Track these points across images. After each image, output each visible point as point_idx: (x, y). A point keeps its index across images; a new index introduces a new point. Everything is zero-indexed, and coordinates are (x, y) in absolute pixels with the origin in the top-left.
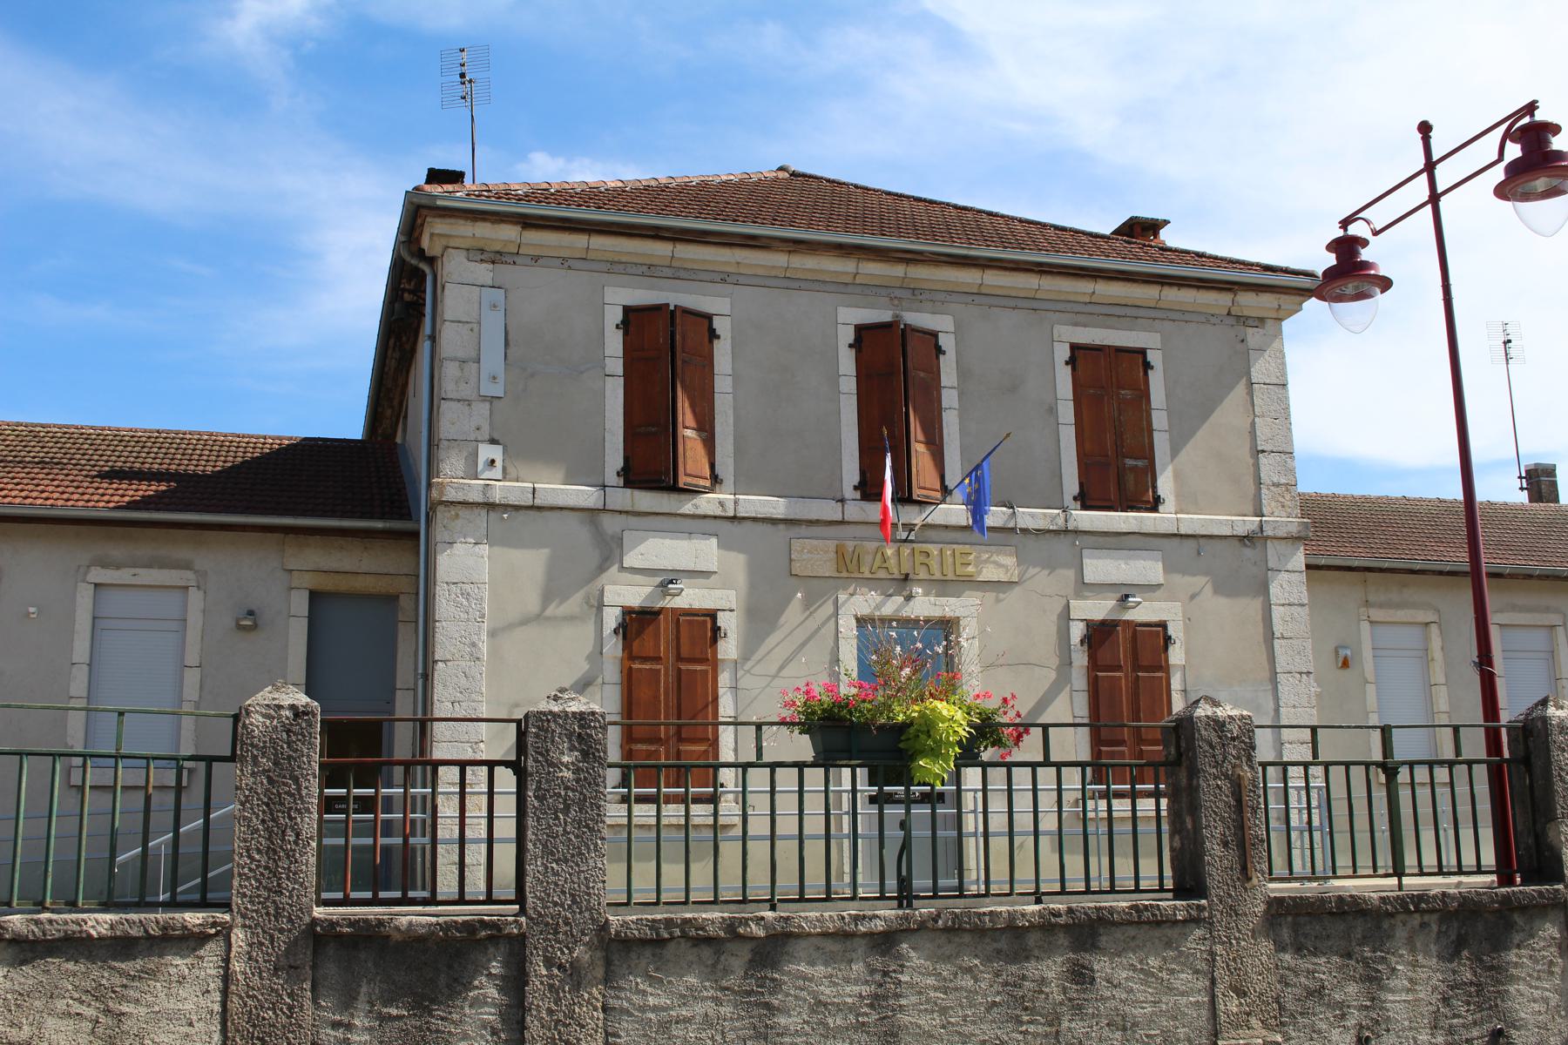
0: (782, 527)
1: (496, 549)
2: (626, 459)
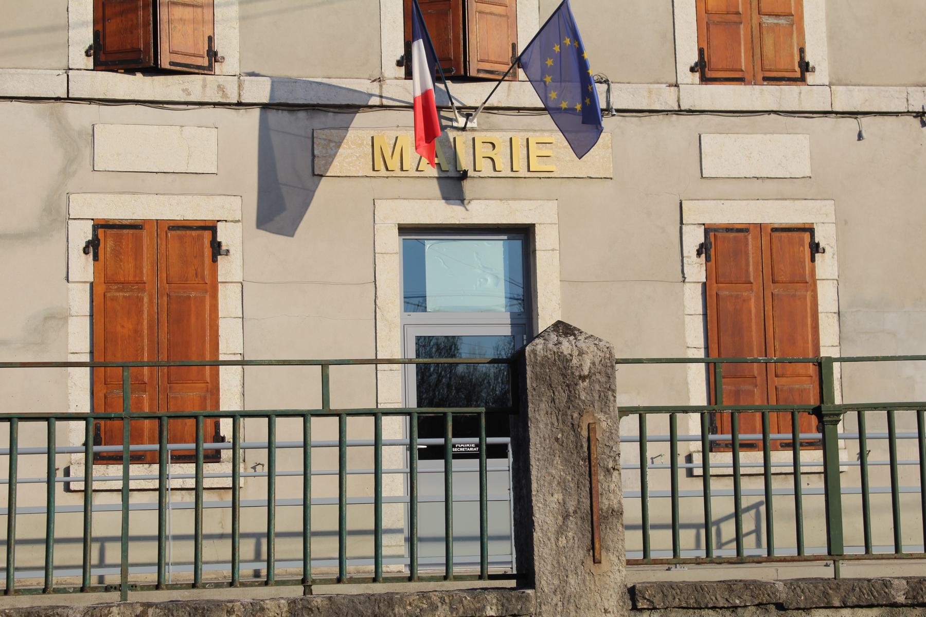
0: (302, 115)
2: (96, 34)
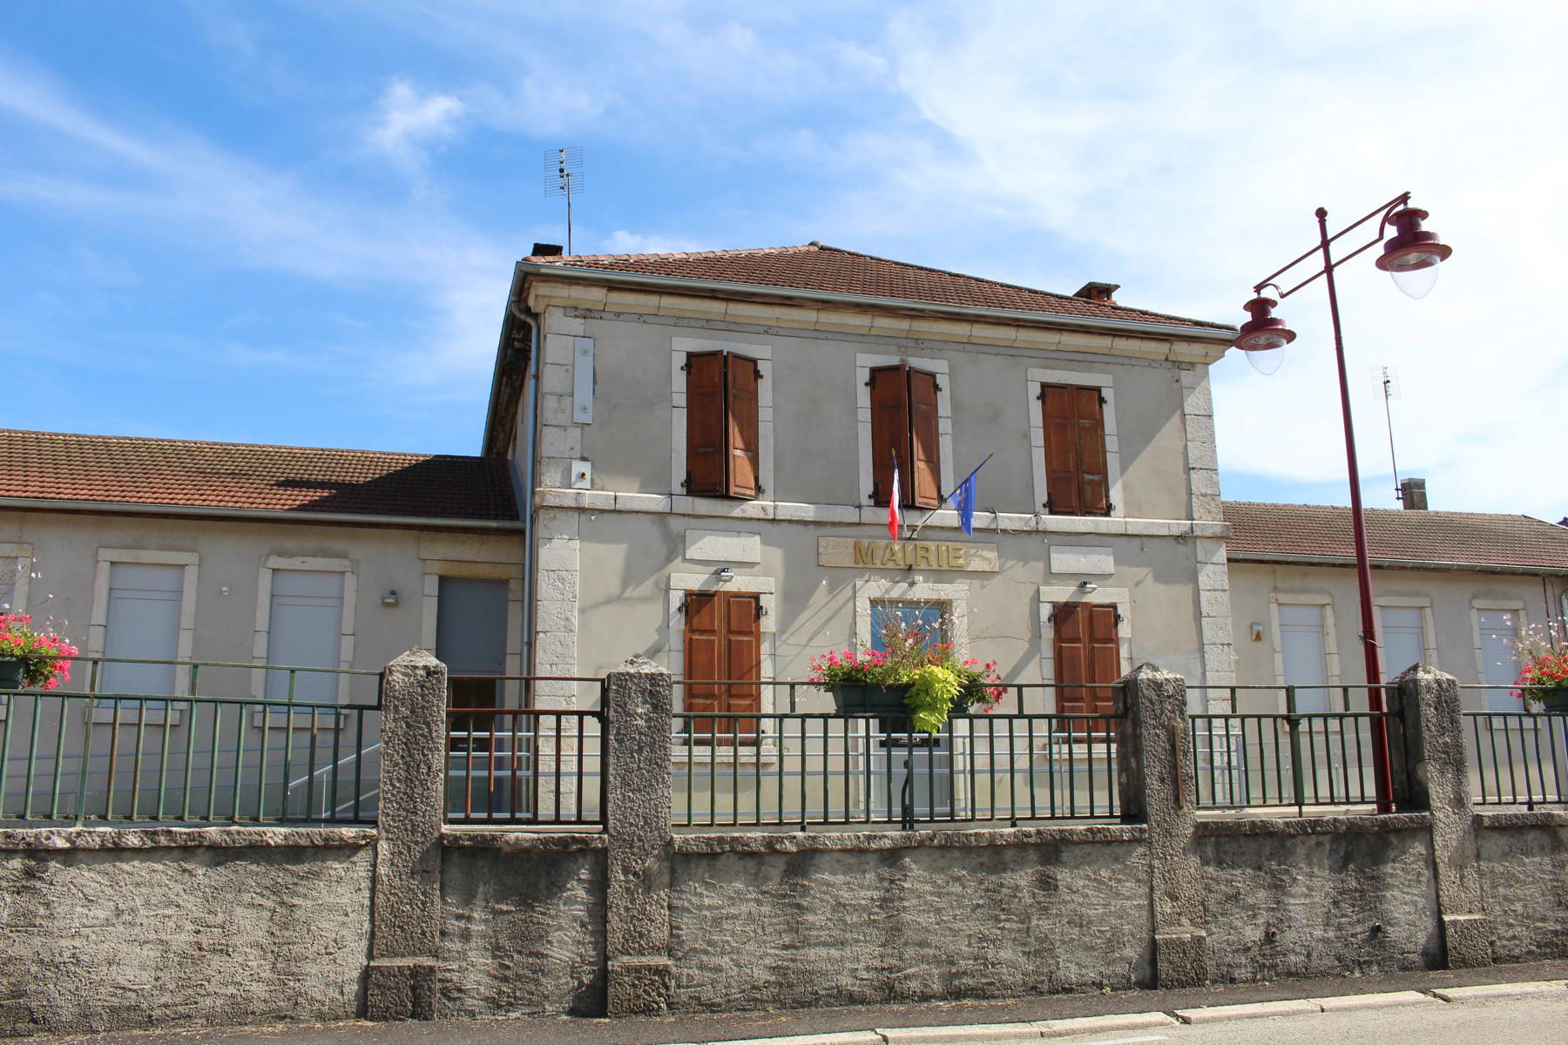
1: (587, 545)
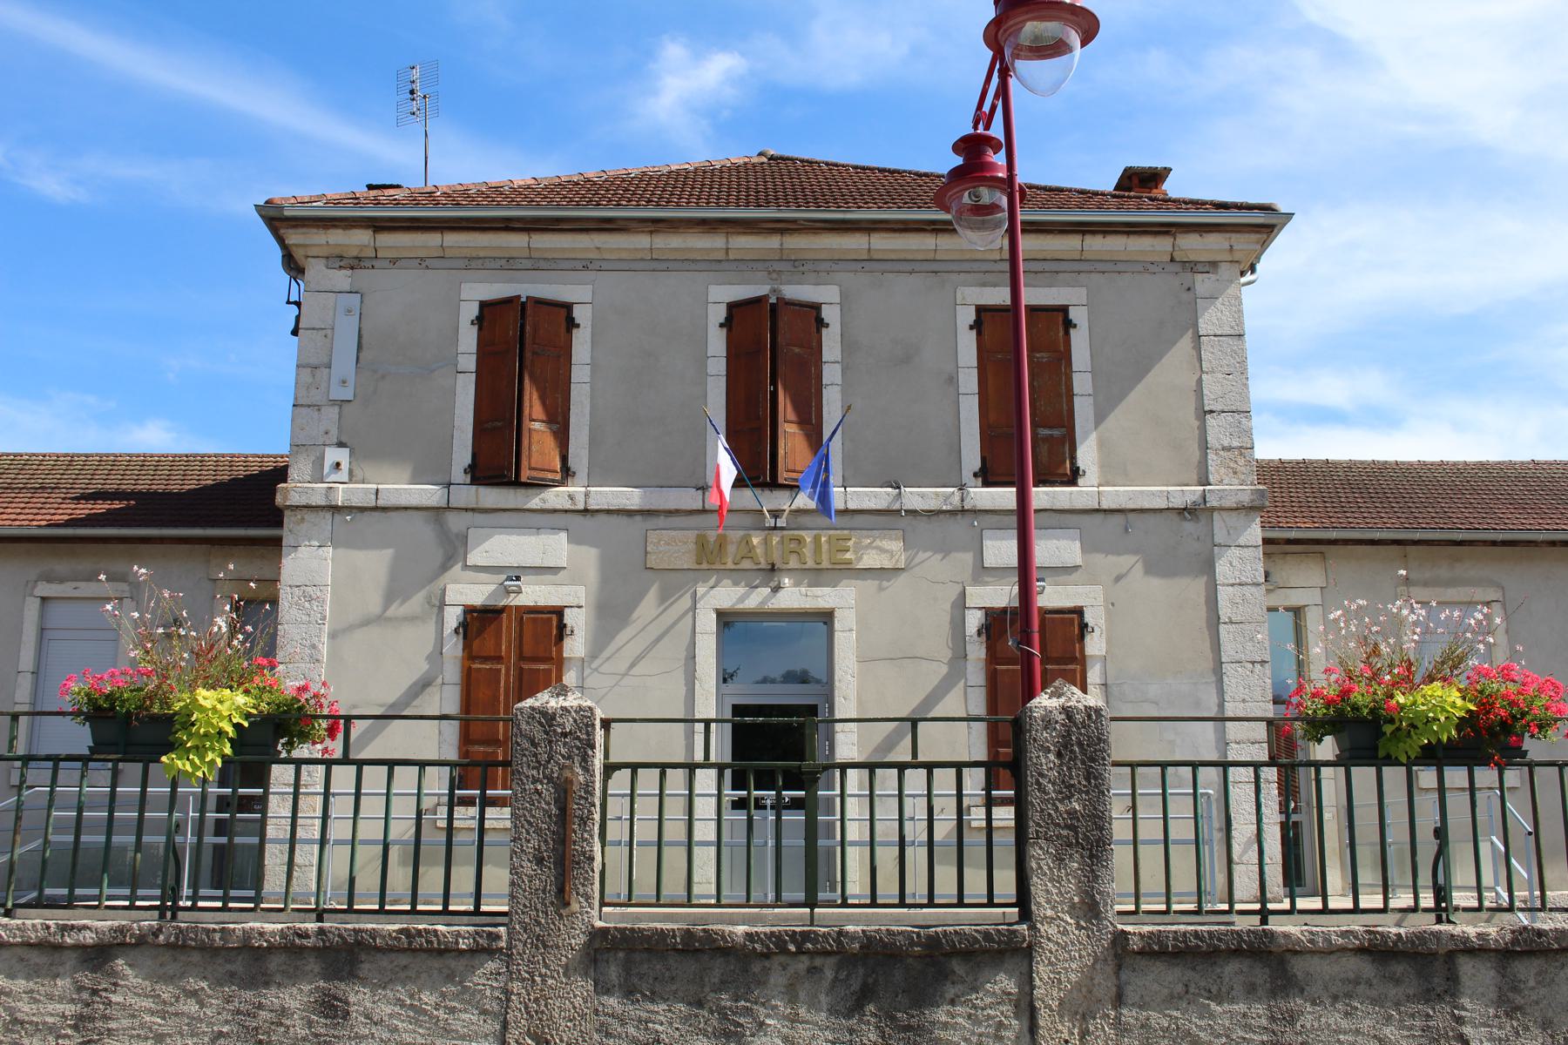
0: (638, 518)
1: (340, 551)
2: (474, 456)
